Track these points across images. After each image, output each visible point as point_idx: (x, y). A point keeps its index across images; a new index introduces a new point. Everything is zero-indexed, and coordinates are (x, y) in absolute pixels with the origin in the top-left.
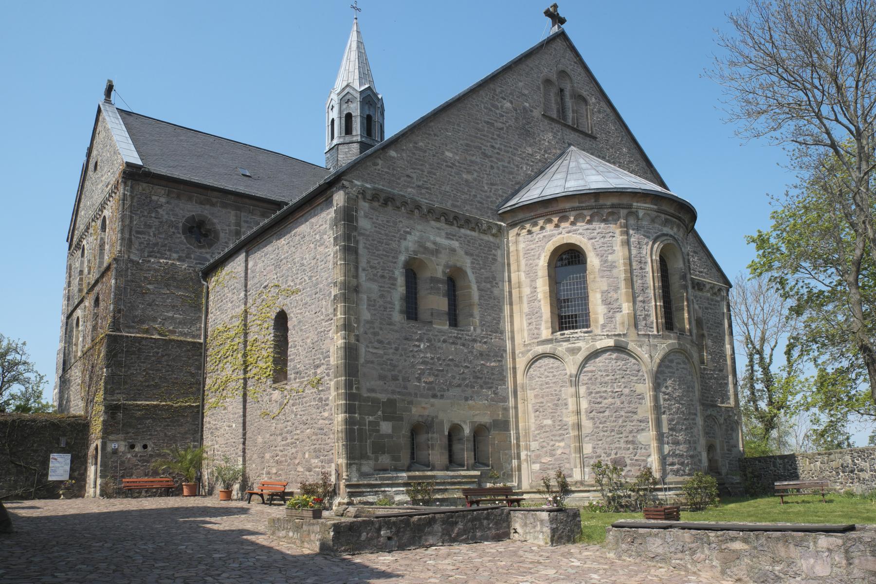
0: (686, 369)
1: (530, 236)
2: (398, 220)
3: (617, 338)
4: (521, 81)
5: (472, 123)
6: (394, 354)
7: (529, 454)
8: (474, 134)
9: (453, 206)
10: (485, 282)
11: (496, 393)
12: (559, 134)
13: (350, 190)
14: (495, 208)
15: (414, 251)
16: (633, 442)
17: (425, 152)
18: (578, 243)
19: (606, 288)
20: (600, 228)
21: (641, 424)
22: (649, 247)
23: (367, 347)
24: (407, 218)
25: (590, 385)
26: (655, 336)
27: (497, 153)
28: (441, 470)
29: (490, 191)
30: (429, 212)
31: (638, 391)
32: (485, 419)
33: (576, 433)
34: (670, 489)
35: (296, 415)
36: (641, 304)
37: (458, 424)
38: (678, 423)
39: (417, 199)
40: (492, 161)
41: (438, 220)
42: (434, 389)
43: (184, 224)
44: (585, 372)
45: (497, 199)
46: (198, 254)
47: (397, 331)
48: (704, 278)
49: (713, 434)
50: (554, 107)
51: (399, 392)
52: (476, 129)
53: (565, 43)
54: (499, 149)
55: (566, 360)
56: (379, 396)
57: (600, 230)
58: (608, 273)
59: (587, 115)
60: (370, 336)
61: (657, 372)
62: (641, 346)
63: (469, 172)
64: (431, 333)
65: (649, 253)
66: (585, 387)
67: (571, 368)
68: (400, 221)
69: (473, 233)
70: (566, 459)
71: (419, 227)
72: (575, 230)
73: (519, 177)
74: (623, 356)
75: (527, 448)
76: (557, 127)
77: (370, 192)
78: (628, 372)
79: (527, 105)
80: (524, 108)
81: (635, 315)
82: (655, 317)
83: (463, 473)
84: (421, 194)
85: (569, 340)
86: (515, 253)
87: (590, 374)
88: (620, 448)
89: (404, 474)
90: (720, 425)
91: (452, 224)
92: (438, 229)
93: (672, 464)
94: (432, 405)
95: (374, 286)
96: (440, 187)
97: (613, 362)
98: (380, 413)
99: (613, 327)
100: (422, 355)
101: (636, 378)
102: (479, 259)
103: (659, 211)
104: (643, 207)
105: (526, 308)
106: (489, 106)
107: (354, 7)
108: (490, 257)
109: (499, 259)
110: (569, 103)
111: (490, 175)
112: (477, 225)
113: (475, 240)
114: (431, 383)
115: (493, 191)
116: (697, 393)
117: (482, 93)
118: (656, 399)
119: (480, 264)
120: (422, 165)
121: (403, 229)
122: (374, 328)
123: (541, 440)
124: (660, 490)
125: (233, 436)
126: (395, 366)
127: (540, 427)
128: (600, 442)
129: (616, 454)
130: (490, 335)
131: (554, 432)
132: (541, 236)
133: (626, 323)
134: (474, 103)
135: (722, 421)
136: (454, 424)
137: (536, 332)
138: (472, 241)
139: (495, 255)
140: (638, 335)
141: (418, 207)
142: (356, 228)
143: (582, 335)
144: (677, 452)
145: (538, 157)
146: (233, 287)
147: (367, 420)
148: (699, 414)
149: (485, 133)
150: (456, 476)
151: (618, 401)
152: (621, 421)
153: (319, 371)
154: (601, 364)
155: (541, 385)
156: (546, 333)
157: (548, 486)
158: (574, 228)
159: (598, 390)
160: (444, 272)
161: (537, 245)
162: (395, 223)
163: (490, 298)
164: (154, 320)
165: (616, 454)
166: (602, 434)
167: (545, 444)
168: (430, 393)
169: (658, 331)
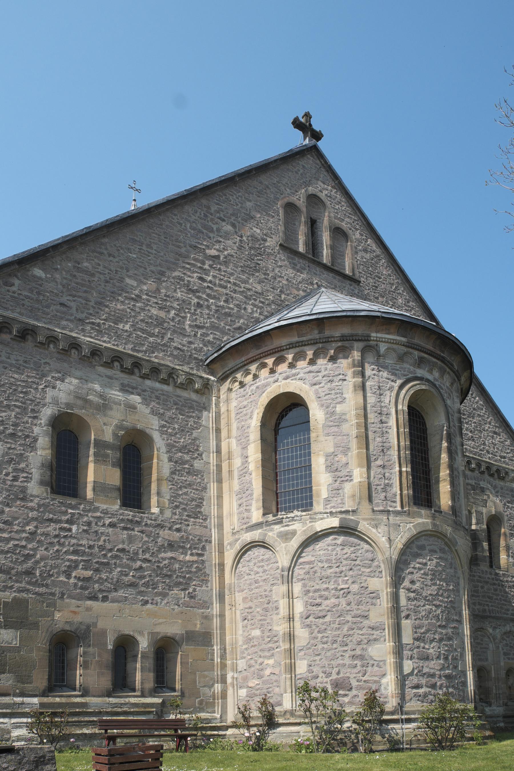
0: (446, 560)
1: (242, 389)
2: (43, 361)
3: (344, 516)
4: (250, 201)
5: (170, 246)
7: (235, 676)
8: (173, 260)
11: (192, 597)
16: (361, 657)
17: (93, 275)
18: (297, 392)
19: (332, 450)
20: (326, 369)
21: (374, 632)
22: (394, 394)
24: (57, 359)
25: (306, 582)
26: (397, 513)
28: (99, 696)
31: (371, 588)
33: (287, 646)
34: (409, 721)
36: (380, 470)
37: (130, 636)
38: (428, 631)
41: (108, 365)
44: (301, 564)
48: (507, 464)
50: (302, 239)
52: (177, 254)
53: (318, 162)
54: (210, 282)
55: (277, 549)
57: (326, 372)
58: (335, 429)
61: (398, 562)
62: (376, 526)
65: (393, 401)
66: (300, 584)
67: (284, 561)
68: (46, 363)
69: (165, 387)
70: (276, 681)
72: (294, 375)
74: (352, 540)
75: (235, 669)
78: (358, 562)
81: (369, 485)
82: (398, 487)
83: (133, 700)
86: (226, 414)
87: (307, 566)
89: (35, 700)
91: (131, 372)
92: (110, 378)
93: (417, 687)
99: (340, 501)
100: (74, 541)
101: (368, 570)
103: (410, 346)
106: (200, 228)
107: (132, 188)
110: (326, 238)
113: (168, 396)
117: (188, 208)
118: (395, 598)
120: (85, 292)
123: (249, 657)
124: (396, 721)
127: (249, 640)
128: (318, 658)
129: (338, 673)
130: (186, 520)
131: (264, 646)
132: (254, 387)
133: (358, 495)
136: (123, 635)
137: (246, 515)
140: (373, 511)
144: (426, 670)
145: (271, 297)
150: (122, 704)
151: (343, 601)
152: (346, 629)
154: (322, 552)
155: (250, 584)
157: (246, 719)
158: (294, 371)
159: (317, 587)
160: (115, 435)
161: (250, 400)
165: (338, 673)
166: (320, 646)
167: (252, 662)
169: (402, 507)
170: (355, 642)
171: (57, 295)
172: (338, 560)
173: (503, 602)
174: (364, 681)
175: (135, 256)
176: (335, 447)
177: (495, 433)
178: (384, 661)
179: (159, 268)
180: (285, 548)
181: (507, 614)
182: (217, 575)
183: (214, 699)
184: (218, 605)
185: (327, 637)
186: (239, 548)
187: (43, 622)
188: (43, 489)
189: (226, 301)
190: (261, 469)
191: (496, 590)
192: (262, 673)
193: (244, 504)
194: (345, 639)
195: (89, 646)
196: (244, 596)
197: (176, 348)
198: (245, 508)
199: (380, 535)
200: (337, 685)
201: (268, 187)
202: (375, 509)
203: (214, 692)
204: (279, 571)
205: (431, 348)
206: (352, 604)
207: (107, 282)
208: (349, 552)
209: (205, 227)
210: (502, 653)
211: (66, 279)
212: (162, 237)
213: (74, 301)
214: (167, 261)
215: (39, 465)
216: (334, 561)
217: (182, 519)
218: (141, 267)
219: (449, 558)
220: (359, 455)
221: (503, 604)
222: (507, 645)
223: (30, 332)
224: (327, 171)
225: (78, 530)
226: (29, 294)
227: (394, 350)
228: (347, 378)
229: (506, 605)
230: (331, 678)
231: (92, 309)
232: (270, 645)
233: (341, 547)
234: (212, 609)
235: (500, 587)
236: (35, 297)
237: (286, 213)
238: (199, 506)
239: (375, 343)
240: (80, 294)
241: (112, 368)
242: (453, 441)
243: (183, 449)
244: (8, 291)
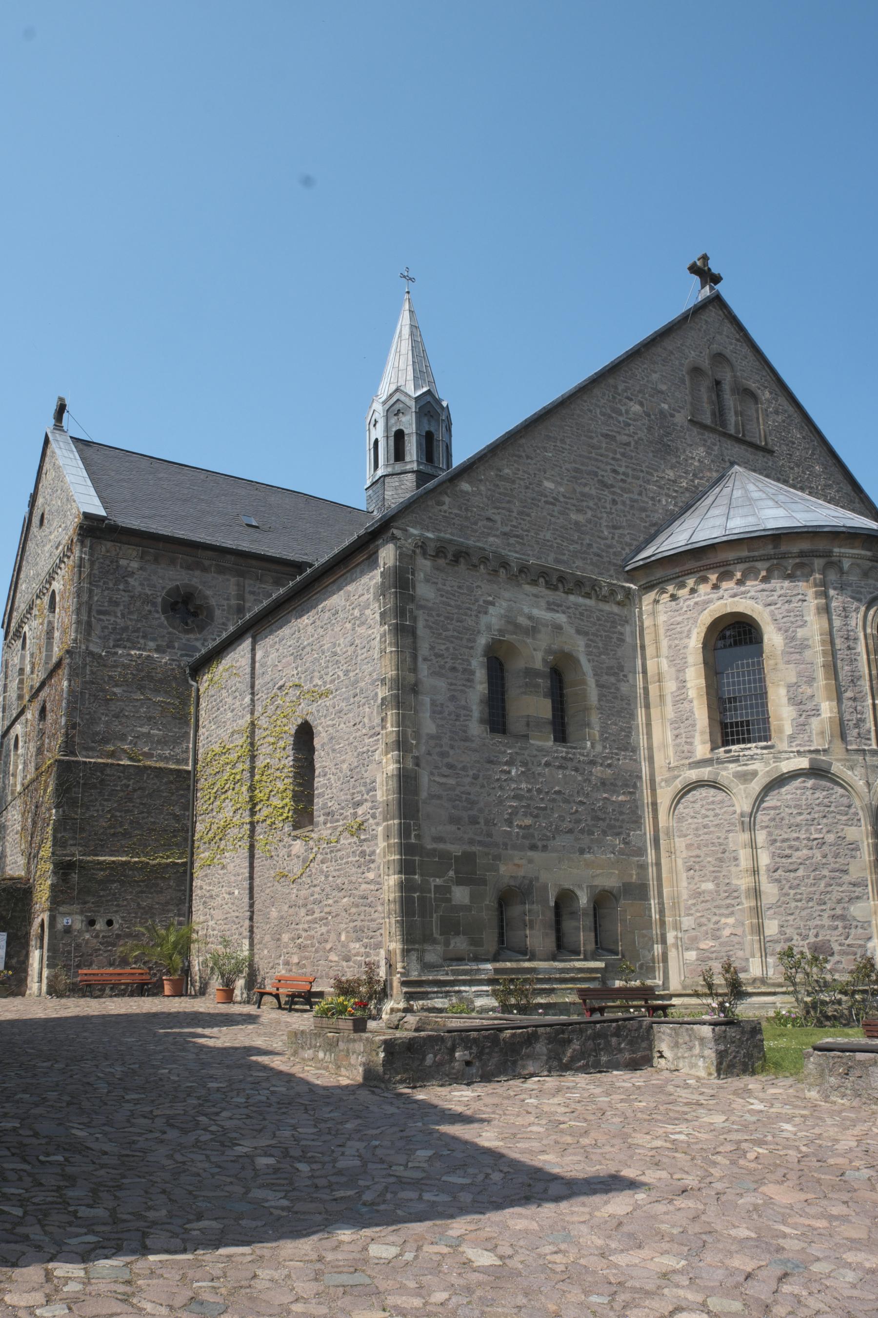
1: (674, 603)
3: (814, 756)
4: (655, 372)
5: (583, 438)
8: (586, 454)
9: (557, 561)
11: (626, 843)
12: (716, 448)
14: (619, 562)
15: (500, 631)
16: (843, 917)
17: (513, 482)
18: (749, 612)
19: (794, 680)
20: (782, 588)
21: (856, 889)
23: (432, 774)
24: (489, 581)
25: (771, 830)
28: (545, 960)
29: (613, 538)
30: (521, 571)
31: (850, 838)
32: (610, 881)
33: (753, 903)
35: (327, 877)
36: (850, 703)
37: (570, 890)
39: (503, 552)
40: (614, 493)
41: (534, 582)
42: (533, 836)
43: (163, 598)
44: (764, 809)
45: (623, 549)
47: (475, 750)
50: (707, 408)
53: (721, 312)
54: (624, 474)
55: (734, 791)
56: (449, 847)
57: (782, 592)
58: (797, 656)
59: (758, 419)
62: (852, 768)
63: (579, 511)
64: (526, 753)
65: (860, 623)
67: (743, 804)
68: (478, 587)
69: (588, 602)
70: (739, 943)
71: (507, 595)
72: (743, 593)
73: (656, 516)
74: (823, 783)
75: (677, 926)
76: (711, 437)
77: (432, 545)
78: (832, 809)
80: (661, 412)
83: (578, 964)
84: (509, 545)
87: (772, 812)
88: (823, 926)
89: (489, 966)
91: (556, 589)
92: (536, 596)
95: (441, 684)
96: (537, 534)
97: (809, 793)
98: (451, 873)
99: (806, 739)
100: (513, 786)
101: (845, 818)
105: (670, 711)
106: (609, 411)
107: (404, 277)
108: (615, 636)
109: (628, 639)
110: (730, 401)
112: (593, 588)
113: (591, 612)
114: (528, 827)
115: (616, 538)
117: (597, 391)
120: (509, 502)
121: (483, 598)
122: (441, 746)
123: (698, 914)
125: (235, 908)
127: (697, 894)
128: (791, 918)
129: (817, 936)
130: (617, 754)
132: (691, 603)
136: (564, 890)
138: (586, 613)
139: (621, 634)
140: (847, 750)
141: (505, 565)
142: (412, 598)
143: (759, 751)
145: (684, 484)
146: (234, 689)
147: (433, 884)
149: (603, 451)
150: (568, 969)
152: (822, 885)
153: (360, 811)
154: (789, 797)
155: (697, 829)
156: (702, 750)
157: (710, 986)
158: (743, 589)
159: (786, 836)
160: (544, 660)
161: (686, 616)
164: (123, 738)
165: (817, 936)
166: (793, 904)
167: (704, 920)
168: (527, 842)
170: (834, 900)
171: (483, 509)
172: (809, 806)
174: (848, 945)
175: (550, 455)
176: (797, 677)
178: (869, 922)
180: (745, 791)
182: (651, 816)
183: (654, 963)
184: (653, 851)
185: (800, 894)
186: (680, 787)
190: (705, 697)
192: (718, 933)
193: (684, 735)
194: (822, 897)
195: (533, 903)
196: (689, 842)
198: (684, 740)
199: (857, 778)
200: (816, 948)
201: (672, 353)
202: (849, 747)
203: (653, 955)
204: (736, 816)
206: (829, 856)
207: (527, 488)
208: (821, 797)
209: (614, 410)
211: (489, 490)
212: (575, 429)
214: (580, 456)
216: (804, 807)
217: (612, 753)
218: (556, 466)
220: (827, 686)
224: (731, 322)
225: (517, 772)
226: (458, 512)
227: (858, 565)
228: (807, 598)
230: (807, 941)
232: (728, 901)
233: (811, 791)
234: (647, 856)
236: (463, 514)
238: (628, 736)
239: (837, 559)
240: (504, 505)
244: (440, 511)
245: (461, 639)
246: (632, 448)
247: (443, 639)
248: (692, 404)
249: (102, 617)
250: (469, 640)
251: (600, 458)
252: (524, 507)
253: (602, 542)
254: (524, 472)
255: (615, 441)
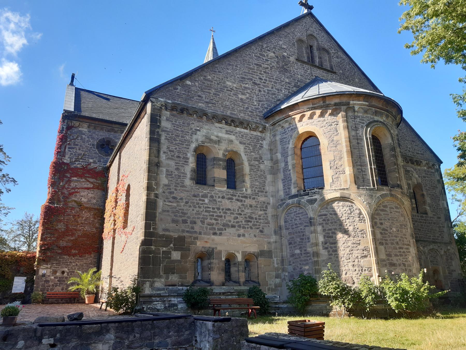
0: (399, 212)
2: (191, 122)
3: (342, 191)
4: (281, 41)
5: (246, 65)
6: (184, 205)
8: (247, 72)
9: (231, 113)
10: (254, 160)
11: (261, 231)
12: (309, 71)
13: (156, 104)
15: (202, 141)
23: (165, 201)
27: (264, 82)
29: (259, 105)
32: (253, 249)
40: (260, 87)
41: (220, 122)
42: (215, 229)
46: (105, 159)
49: (437, 262)
51: (187, 231)
53: (312, 19)
54: (265, 80)
56: (172, 234)
60: (167, 194)
63: (243, 94)
64: (213, 192)
69: (246, 131)
71: (206, 127)
73: (280, 97)
76: (306, 66)
77: (170, 105)
79: (286, 54)
80: (283, 56)
84: (208, 107)
85: (308, 195)
87: (324, 217)
90: (441, 256)
91: (231, 125)
94: (213, 240)
95: (172, 163)
98: (172, 245)
100: (205, 206)
102: (250, 146)
104: (357, 104)
107: (211, 30)
108: (258, 145)
110: (316, 53)
111: (258, 95)
112: (248, 125)
113: (247, 135)
115: (260, 105)
116: (409, 230)
119: (250, 150)
120: (209, 89)
126: (185, 214)
127: (293, 255)
132: (290, 129)
134: (248, 54)
135: (442, 253)
138: (244, 135)
139: (262, 144)
141: (206, 114)
142: (159, 127)
148: (412, 245)
149: (255, 71)
155: (292, 226)
159: (330, 228)
162: (189, 124)
163: (258, 170)
168: (212, 232)
169: (374, 186)
171: (197, 92)
173: (427, 232)
175: (230, 71)
177: (413, 141)
179: (241, 76)
180: (311, 208)
181: (430, 239)
187: (192, 247)
188: (192, 182)
189: (272, 88)
191: (422, 225)
195: (214, 259)
196: (290, 232)
197: (250, 112)
198: (287, 187)
205: (381, 106)
207: (218, 84)
209: (261, 54)
210: (429, 261)
211: (200, 84)
213: (204, 94)
214: (244, 72)
215: (190, 170)
218: (233, 76)
219: (401, 211)
221: (427, 233)
222: (432, 256)
223: (185, 110)
229: (428, 233)
231: (212, 97)
235: (424, 224)
237: (298, 44)
240: (207, 91)
241: (221, 124)
242: (396, 151)
243: (256, 159)
245: (183, 145)
246: (269, 70)
247: (174, 144)
248: (298, 53)
249: (70, 150)
250: (186, 145)
251: (253, 73)
252: (217, 92)
253: (254, 107)
254: (217, 78)
255: (261, 67)
